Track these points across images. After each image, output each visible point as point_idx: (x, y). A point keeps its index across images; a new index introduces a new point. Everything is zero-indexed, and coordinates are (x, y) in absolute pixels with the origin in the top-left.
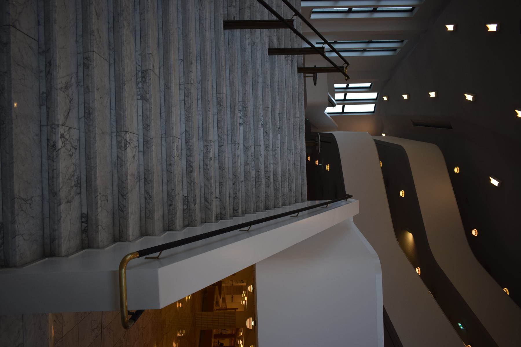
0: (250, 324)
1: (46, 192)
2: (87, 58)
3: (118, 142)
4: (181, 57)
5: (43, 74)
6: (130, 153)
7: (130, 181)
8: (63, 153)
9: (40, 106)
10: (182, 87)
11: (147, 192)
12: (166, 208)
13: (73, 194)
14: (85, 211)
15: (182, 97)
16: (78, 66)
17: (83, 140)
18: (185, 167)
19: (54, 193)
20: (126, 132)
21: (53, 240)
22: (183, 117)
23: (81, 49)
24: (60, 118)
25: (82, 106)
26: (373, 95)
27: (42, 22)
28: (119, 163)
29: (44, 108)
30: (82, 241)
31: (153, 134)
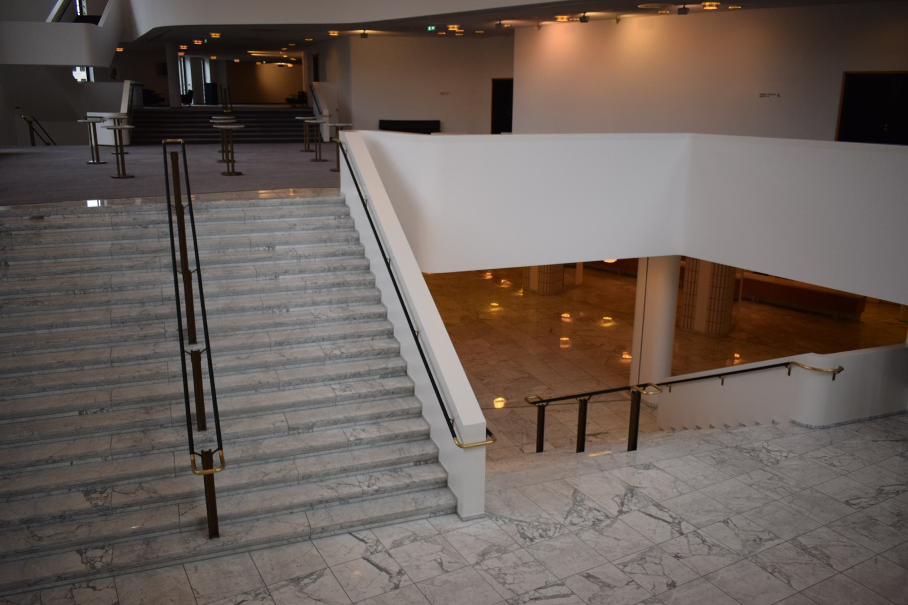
0: (566, 342)
3: (356, 445)
4: (254, 392)
5: (327, 505)
6: (363, 435)
7: (385, 433)
9: (349, 503)
10: (282, 388)
11: (388, 416)
13: (403, 474)
14: (412, 464)
15: (291, 387)
16: (308, 482)
17: (362, 472)
18: (355, 379)
19: (407, 486)
20: (349, 441)
22: (310, 385)
23: (296, 482)
25: (339, 476)
27: (189, 500)
28: (372, 442)
29: (350, 501)
30: (432, 463)
31: (341, 416)
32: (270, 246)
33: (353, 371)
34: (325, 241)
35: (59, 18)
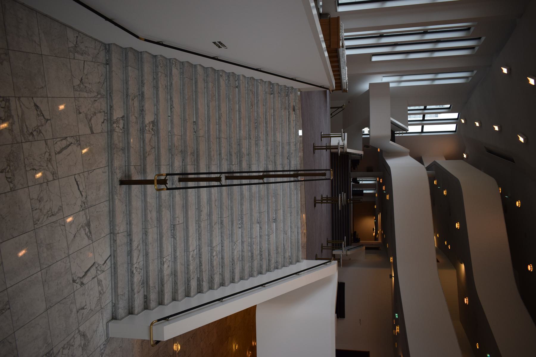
1: (130, 289)
2: (146, 231)
3: (161, 262)
4: (197, 207)
6: (166, 266)
8: (136, 275)
9: (128, 256)
12: (186, 285)
14: (145, 294)
15: (197, 228)
17: (145, 264)
18: (198, 263)
19: (133, 290)
21: (132, 308)
24: (135, 261)
26: (455, 115)
28: (161, 271)
29: (129, 257)
31: (178, 254)
32: (275, 220)
33: (203, 262)
34: (277, 250)
35: (392, 123)
